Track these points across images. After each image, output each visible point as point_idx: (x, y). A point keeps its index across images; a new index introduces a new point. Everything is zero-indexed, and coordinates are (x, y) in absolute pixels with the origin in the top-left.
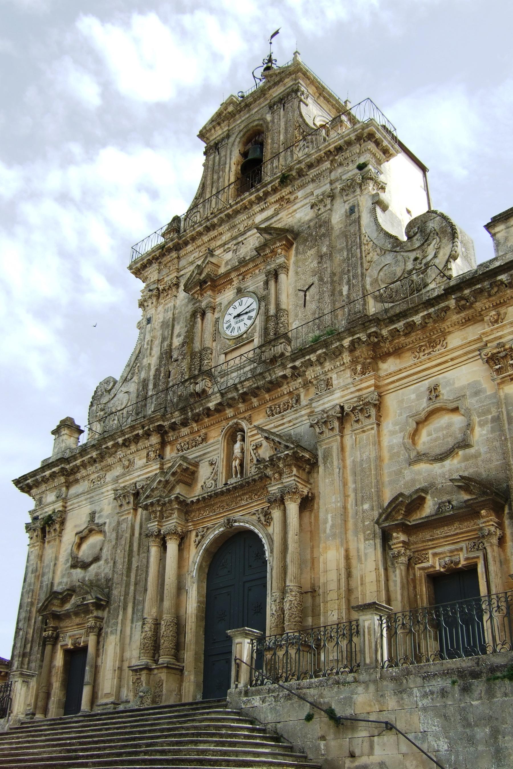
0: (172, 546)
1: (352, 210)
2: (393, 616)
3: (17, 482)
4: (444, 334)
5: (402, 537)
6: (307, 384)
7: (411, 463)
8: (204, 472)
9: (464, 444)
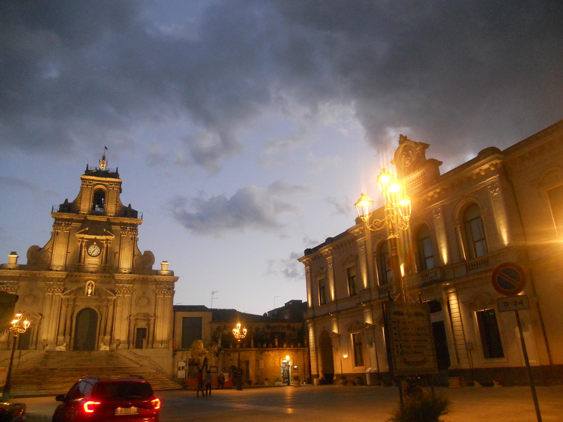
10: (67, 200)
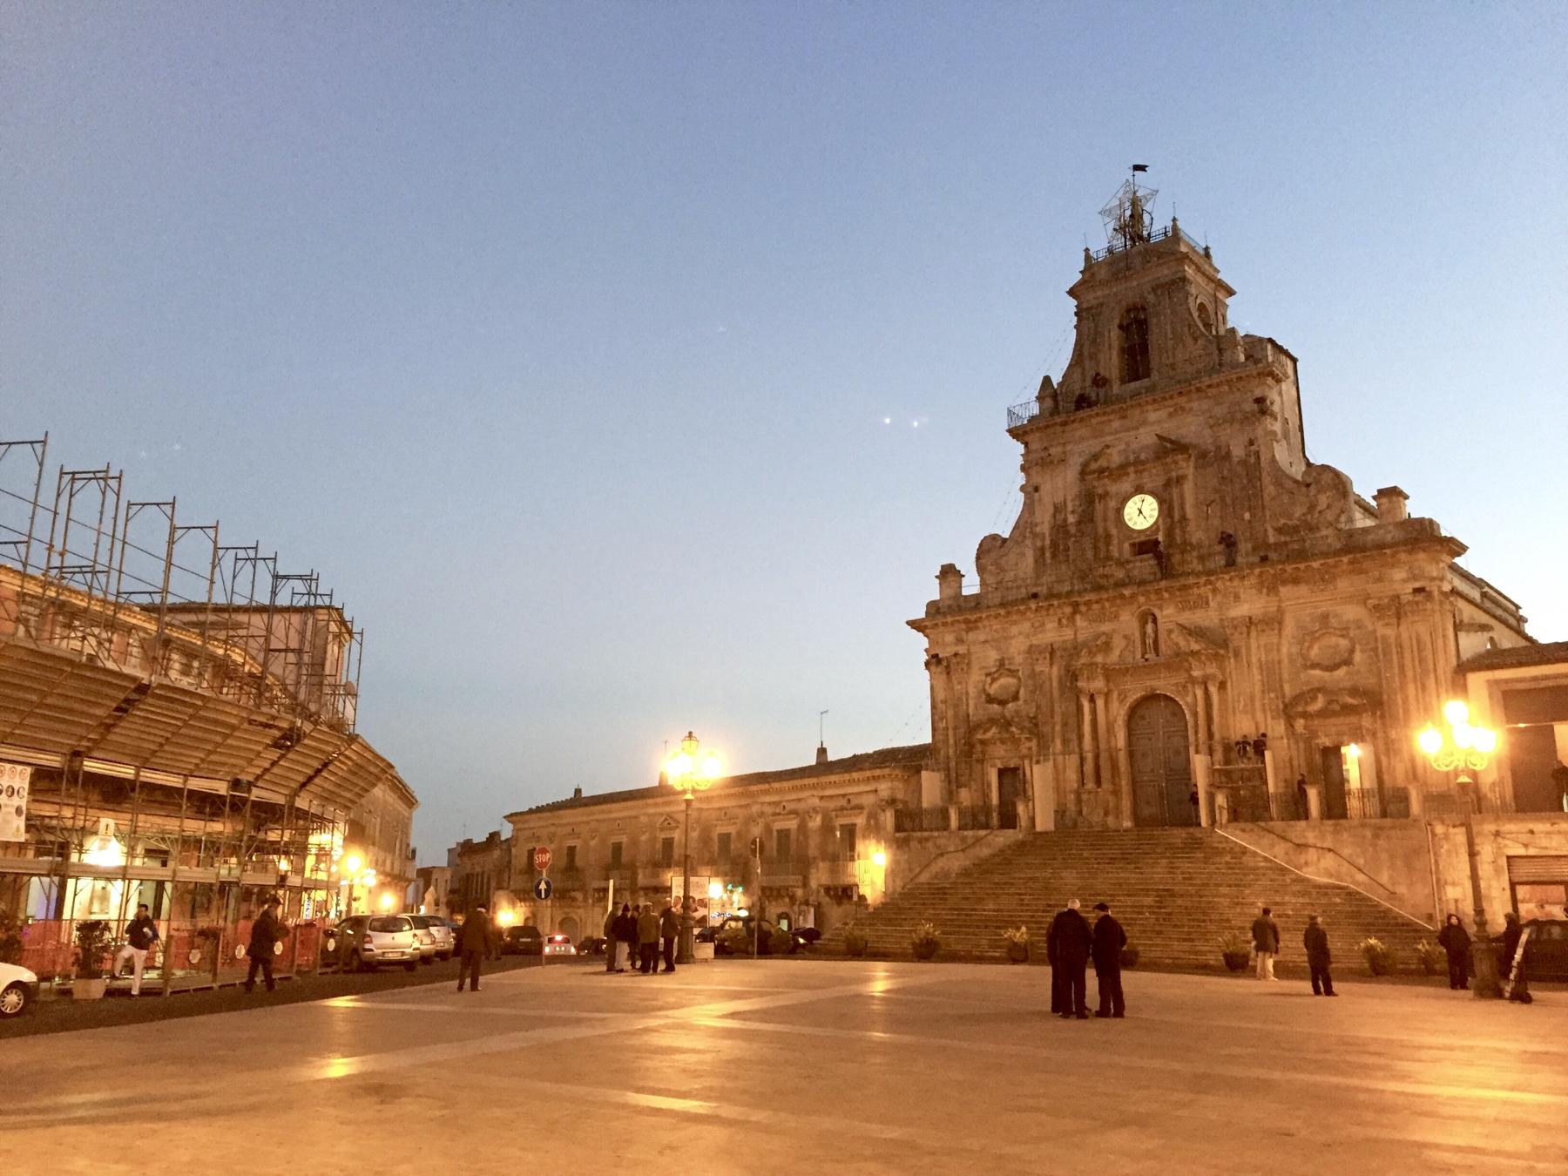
0: (1100, 702)
1: (1251, 443)
2: (577, 884)
3: (908, 623)
4: (1334, 578)
5: (1302, 721)
6: (1215, 591)
7: (1306, 667)
8: (1118, 644)
9: (1347, 662)
10: (1047, 380)
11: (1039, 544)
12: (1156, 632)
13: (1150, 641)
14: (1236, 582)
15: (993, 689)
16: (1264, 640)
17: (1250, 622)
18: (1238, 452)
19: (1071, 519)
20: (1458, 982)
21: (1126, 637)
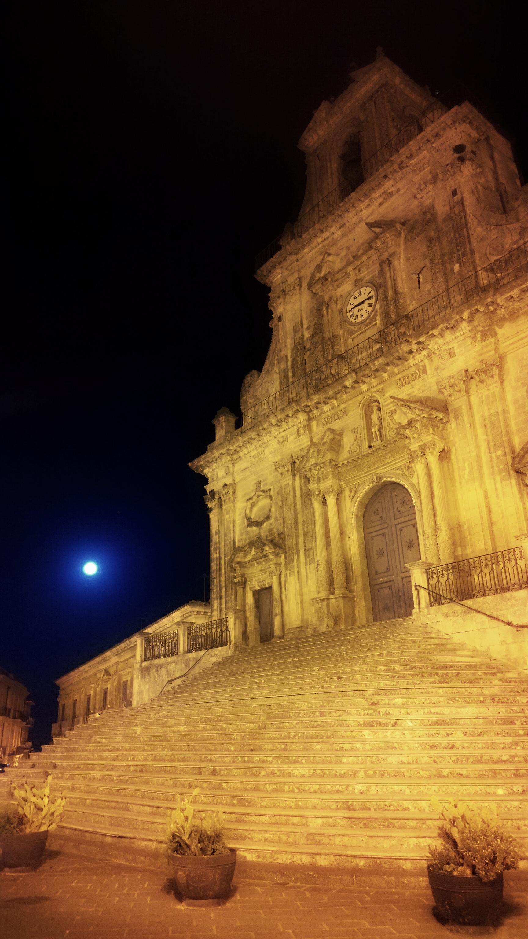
0: (331, 501)
1: (454, 193)
11: (283, 366)
12: (380, 419)
13: (375, 429)
14: (448, 336)
15: (255, 515)
16: (484, 392)
17: (468, 376)
18: (441, 209)
19: (307, 335)
20: (410, 576)
21: (354, 432)
